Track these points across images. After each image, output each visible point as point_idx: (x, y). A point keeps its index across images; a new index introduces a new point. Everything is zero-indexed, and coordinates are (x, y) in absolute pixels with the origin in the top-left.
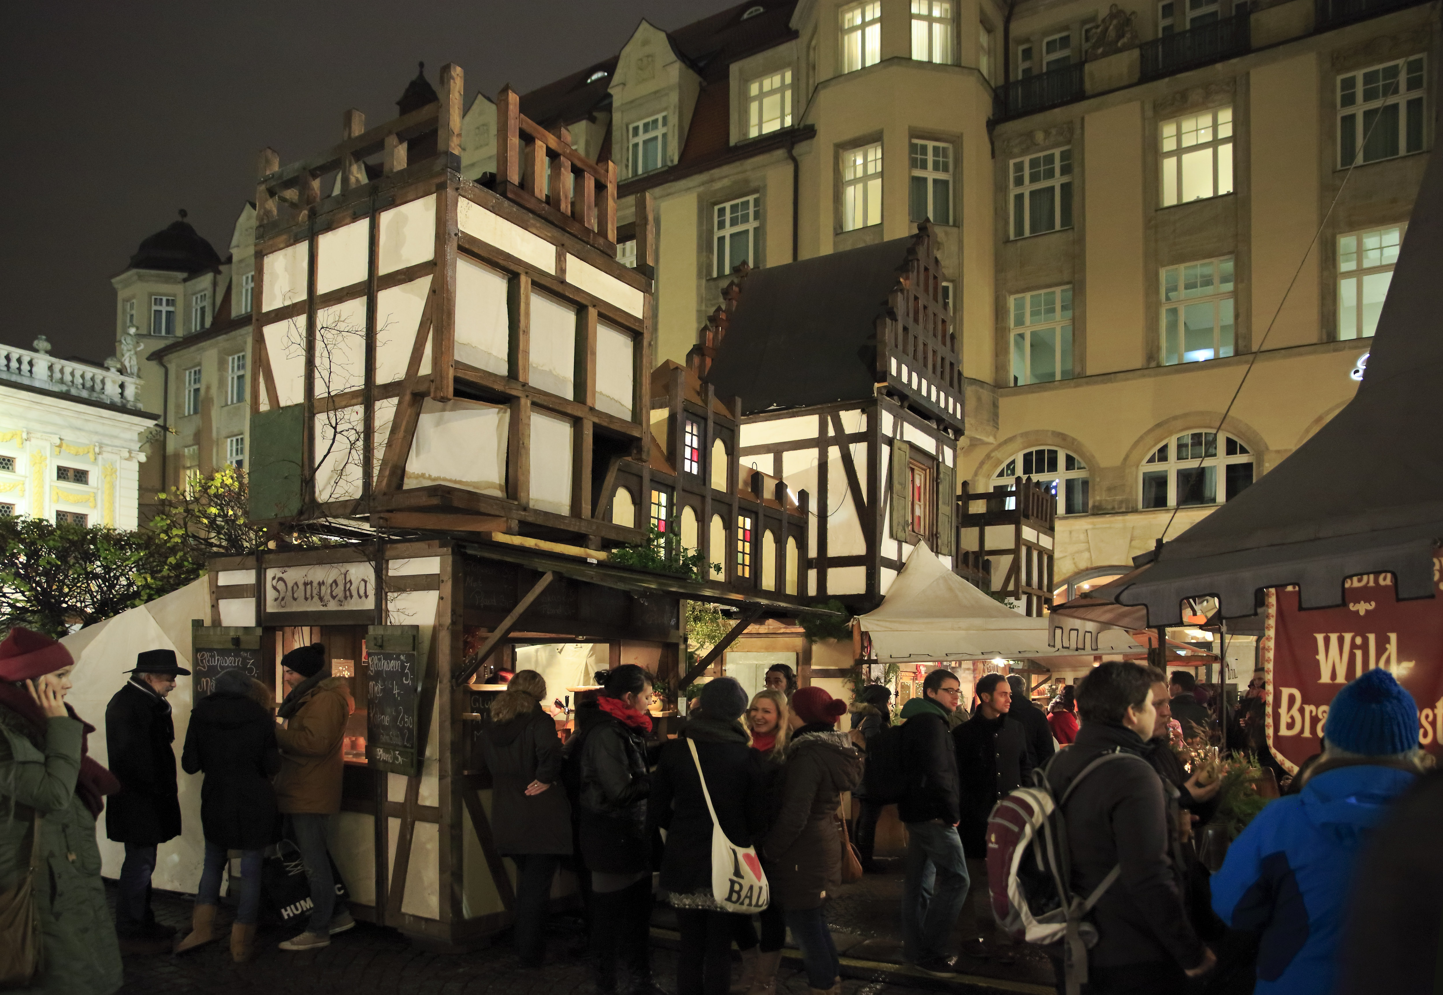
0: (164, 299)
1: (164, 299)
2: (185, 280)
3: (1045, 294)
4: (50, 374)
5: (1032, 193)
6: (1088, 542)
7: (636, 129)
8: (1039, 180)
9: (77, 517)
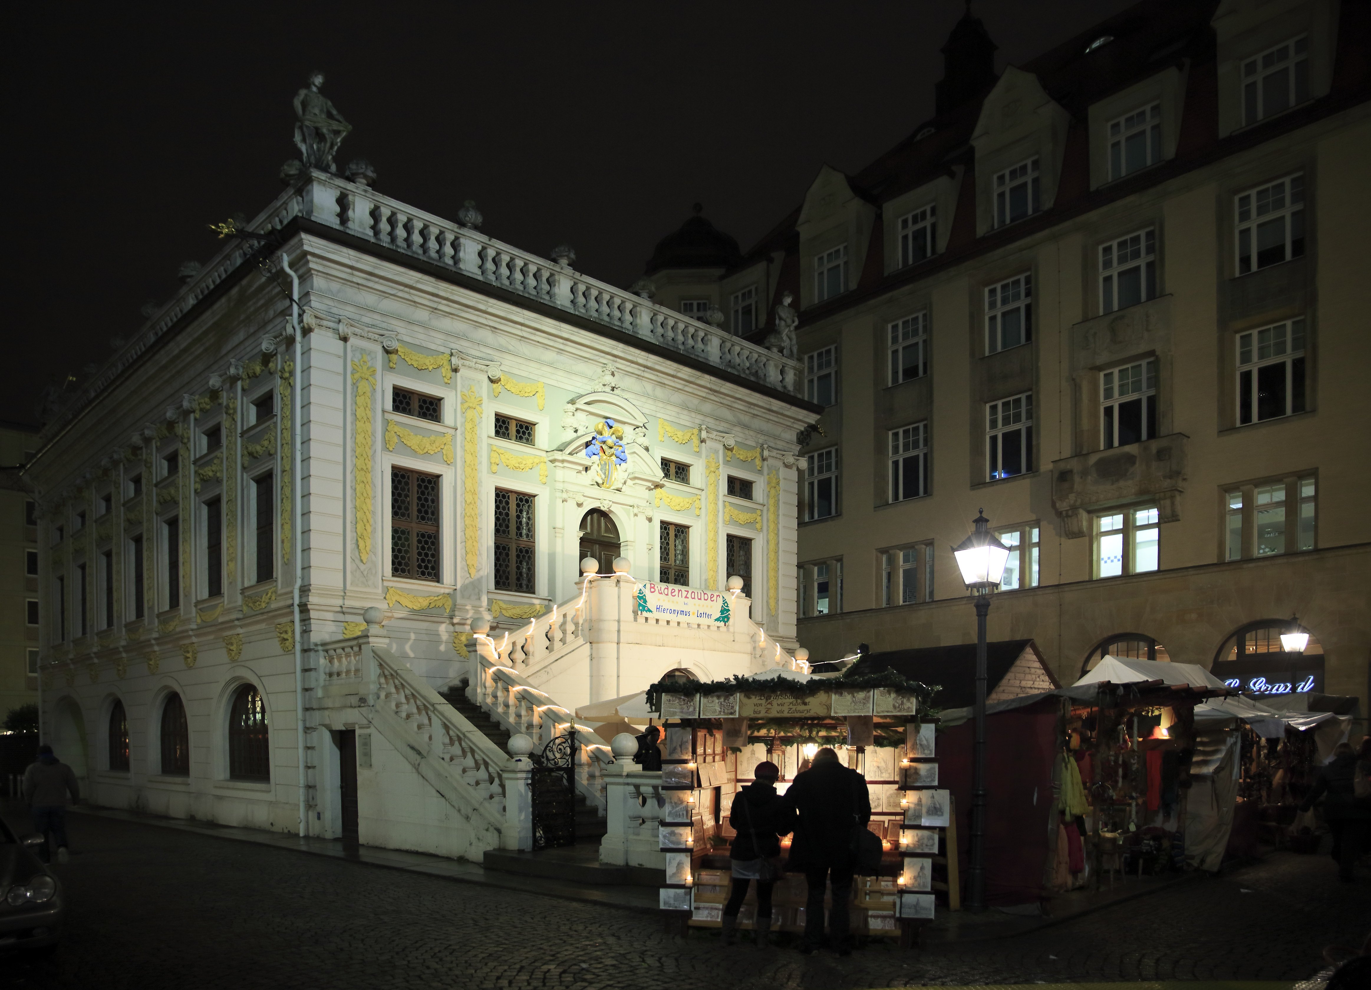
0: (695, 303)
1: (695, 303)
2: (722, 278)
3: (1132, 368)
4: (480, 263)
5: (1004, 315)
6: (717, 571)
7: (1001, 178)
8: (1127, 261)
9: (521, 427)
